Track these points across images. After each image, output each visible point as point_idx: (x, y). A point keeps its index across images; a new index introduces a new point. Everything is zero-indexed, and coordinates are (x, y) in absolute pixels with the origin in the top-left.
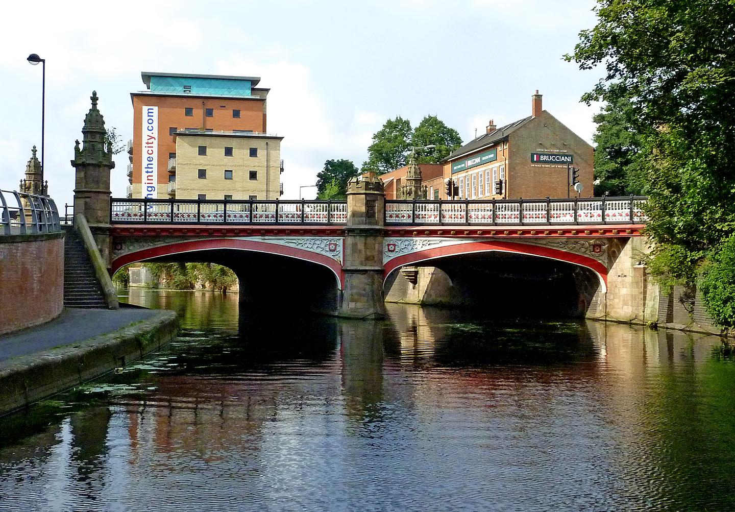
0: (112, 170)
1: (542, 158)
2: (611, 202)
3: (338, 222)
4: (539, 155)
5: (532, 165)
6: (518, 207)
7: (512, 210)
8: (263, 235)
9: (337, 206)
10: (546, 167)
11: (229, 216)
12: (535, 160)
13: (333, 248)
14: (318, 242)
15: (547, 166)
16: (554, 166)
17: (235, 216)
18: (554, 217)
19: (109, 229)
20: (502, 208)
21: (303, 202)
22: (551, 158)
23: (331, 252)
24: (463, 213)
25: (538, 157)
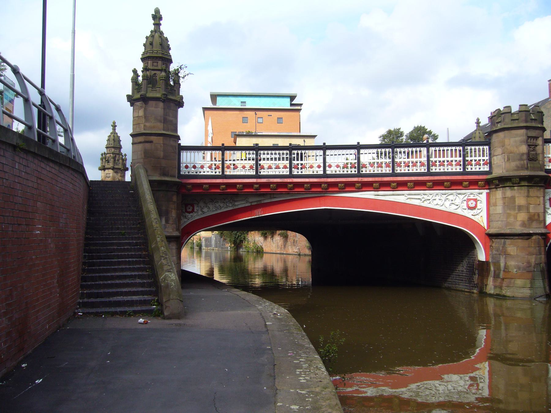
0: (180, 110)
8: (377, 189)
9: (301, 154)
11: (330, 166)
13: (473, 205)
14: (451, 197)
17: (194, 167)
18: (436, 166)
19: (175, 183)
20: (381, 153)
21: (358, 147)
23: (470, 211)
24: (219, 163)
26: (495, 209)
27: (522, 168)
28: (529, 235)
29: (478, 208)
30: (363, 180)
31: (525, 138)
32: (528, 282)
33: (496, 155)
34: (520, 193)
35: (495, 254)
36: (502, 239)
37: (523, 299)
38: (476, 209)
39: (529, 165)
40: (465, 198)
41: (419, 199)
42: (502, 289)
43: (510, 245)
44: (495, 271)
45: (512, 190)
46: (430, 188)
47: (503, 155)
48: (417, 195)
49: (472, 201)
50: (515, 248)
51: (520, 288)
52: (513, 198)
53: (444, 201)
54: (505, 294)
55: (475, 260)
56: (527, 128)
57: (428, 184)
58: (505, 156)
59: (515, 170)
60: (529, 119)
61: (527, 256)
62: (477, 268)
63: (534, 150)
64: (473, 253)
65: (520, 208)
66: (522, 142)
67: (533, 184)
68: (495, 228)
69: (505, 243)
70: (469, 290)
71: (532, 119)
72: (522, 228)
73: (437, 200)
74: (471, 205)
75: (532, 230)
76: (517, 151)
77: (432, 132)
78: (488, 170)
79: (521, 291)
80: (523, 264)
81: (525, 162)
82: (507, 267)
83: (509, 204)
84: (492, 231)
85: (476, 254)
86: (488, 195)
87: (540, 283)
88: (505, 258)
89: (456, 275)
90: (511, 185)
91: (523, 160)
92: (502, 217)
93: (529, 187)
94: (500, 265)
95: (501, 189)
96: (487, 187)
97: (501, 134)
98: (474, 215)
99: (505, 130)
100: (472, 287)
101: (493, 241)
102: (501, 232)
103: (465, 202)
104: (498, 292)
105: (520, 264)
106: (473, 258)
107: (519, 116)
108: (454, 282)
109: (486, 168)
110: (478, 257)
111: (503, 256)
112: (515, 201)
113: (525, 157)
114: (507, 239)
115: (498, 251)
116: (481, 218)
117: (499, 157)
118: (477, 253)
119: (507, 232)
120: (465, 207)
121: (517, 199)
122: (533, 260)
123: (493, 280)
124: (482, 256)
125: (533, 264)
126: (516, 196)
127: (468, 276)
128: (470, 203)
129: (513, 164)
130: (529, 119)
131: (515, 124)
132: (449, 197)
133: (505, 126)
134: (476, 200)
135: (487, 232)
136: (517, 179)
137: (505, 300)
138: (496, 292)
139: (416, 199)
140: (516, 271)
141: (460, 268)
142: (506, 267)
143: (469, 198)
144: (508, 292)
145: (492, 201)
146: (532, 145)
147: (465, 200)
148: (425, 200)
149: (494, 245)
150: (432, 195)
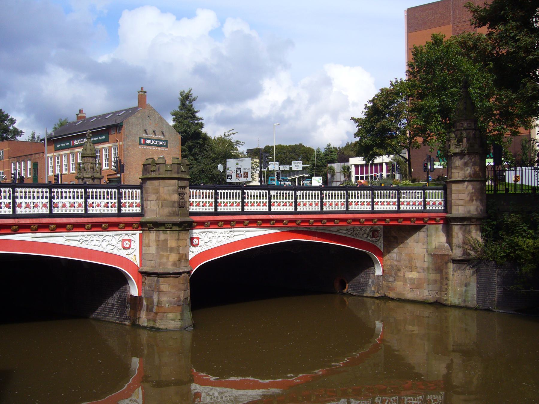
1: (148, 142)
2: (405, 192)
3: (434, 209)
4: (145, 139)
5: (140, 147)
6: (395, 195)
7: (74, 198)
8: (34, 231)
10: (150, 149)
12: (142, 143)
13: (128, 246)
14: (107, 238)
15: (150, 148)
16: (155, 148)
22: (153, 142)
23: (125, 250)
25: (144, 141)
26: (148, 249)
27: (175, 214)
28: (180, 274)
29: (132, 248)
30: (20, 222)
31: (177, 187)
32: (179, 314)
33: (151, 200)
34: (172, 237)
35: (148, 290)
36: (156, 277)
37: (174, 330)
38: (130, 249)
39: (179, 212)
40: (121, 239)
41: (77, 240)
42: (155, 323)
43: (163, 282)
44: (148, 306)
45: (165, 234)
46: (89, 230)
47: (158, 201)
48: (75, 236)
49: (127, 242)
50: (167, 285)
51: (172, 320)
52: (166, 241)
53: (101, 241)
54: (159, 327)
55: (127, 294)
56: (179, 179)
57: (87, 226)
58: (159, 202)
59: (168, 216)
60: (180, 171)
61: (177, 292)
62: (130, 302)
63: (183, 198)
64: (125, 288)
65: (172, 249)
66: (174, 191)
67: (183, 228)
68: (148, 267)
69: (158, 281)
70: (120, 322)
71: (182, 171)
72: (174, 268)
73: (95, 241)
74: (126, 246)
75: (182, 269)
76: (170, 199)
77: (9, 116)
78: (140, 212)
79: (172, 323)
80: (174, 299)
81: (177, 209)
82: (160, 303)
83: (162, 246)
84: (145, 269)
85: (128, 289)
86: (141, 236)
87: (188, 315)
88: (159, 294)
89: (106, 307)
90: (164, 229)
91: (175, 207)
92: (155, 257)
93: (179, 232)
94: (153, 301)
95: (155, 232)
96: (140, 228)
97: (156, 182)
98: (128, 255)
99: (159, 180)
100: (124, 319)
101: (145, 278)
102: (155, 272)
103: (121, 242)
104: (152, 325)
105: (172, 299)
106: (125, 292)
107: (172, 167)
108: (103, 313)
109: (138, 210)
110: (131, 292)
111: (156, 293)
112: (167, 244)
113: (176, 205)
114: (159, 277)
115: (150, 288)
116: (134, 256)
117: (153, 202)
118: (129, 288)
119: (161, 272)
120: (121, 247)
121: (169, 242)
122: (182, 295)
123: (146, 313)
124: (134, 291)
125: (182, 299)
126: (168, 239)
127: (120, 309)
128: (125, 243)
129: (166, 211)
130: (180, 171)
131: (169, 175)
132: (106, 238)
133: (160, 176)
134: (130, 241)
135: (140, 270)
136: (170, 225)
137: (159, 333)
138: (150, 325)
139: (75, 240)
140: (168, 306)
141: (110, 301)
142: (159, 302)
143: (124, 238)
144: (161, 325)
145: (145, 240)
146: (181, 194)
147: (121, 241)
148: (83, 242)
149: (146, 281)
150: (90, 236)
